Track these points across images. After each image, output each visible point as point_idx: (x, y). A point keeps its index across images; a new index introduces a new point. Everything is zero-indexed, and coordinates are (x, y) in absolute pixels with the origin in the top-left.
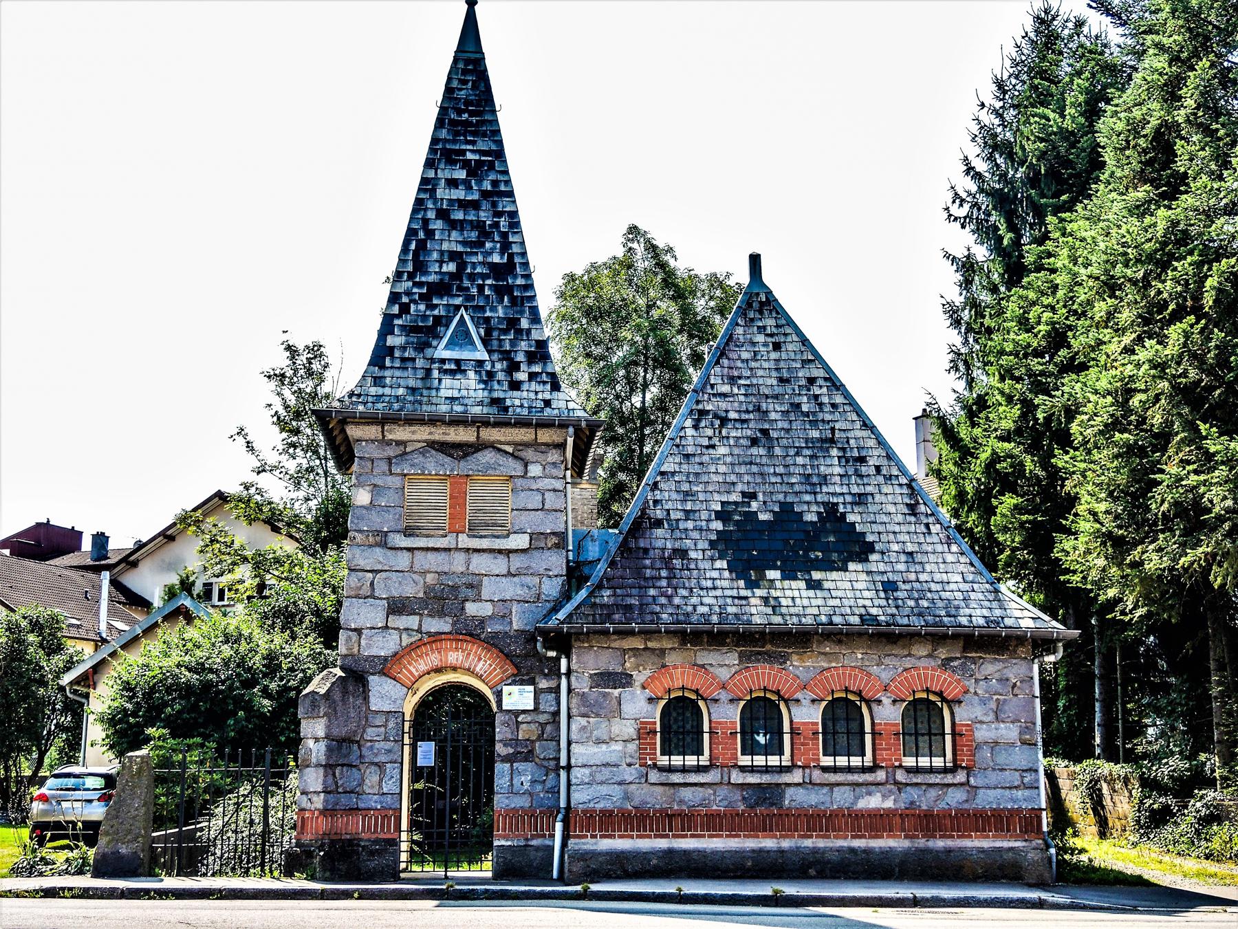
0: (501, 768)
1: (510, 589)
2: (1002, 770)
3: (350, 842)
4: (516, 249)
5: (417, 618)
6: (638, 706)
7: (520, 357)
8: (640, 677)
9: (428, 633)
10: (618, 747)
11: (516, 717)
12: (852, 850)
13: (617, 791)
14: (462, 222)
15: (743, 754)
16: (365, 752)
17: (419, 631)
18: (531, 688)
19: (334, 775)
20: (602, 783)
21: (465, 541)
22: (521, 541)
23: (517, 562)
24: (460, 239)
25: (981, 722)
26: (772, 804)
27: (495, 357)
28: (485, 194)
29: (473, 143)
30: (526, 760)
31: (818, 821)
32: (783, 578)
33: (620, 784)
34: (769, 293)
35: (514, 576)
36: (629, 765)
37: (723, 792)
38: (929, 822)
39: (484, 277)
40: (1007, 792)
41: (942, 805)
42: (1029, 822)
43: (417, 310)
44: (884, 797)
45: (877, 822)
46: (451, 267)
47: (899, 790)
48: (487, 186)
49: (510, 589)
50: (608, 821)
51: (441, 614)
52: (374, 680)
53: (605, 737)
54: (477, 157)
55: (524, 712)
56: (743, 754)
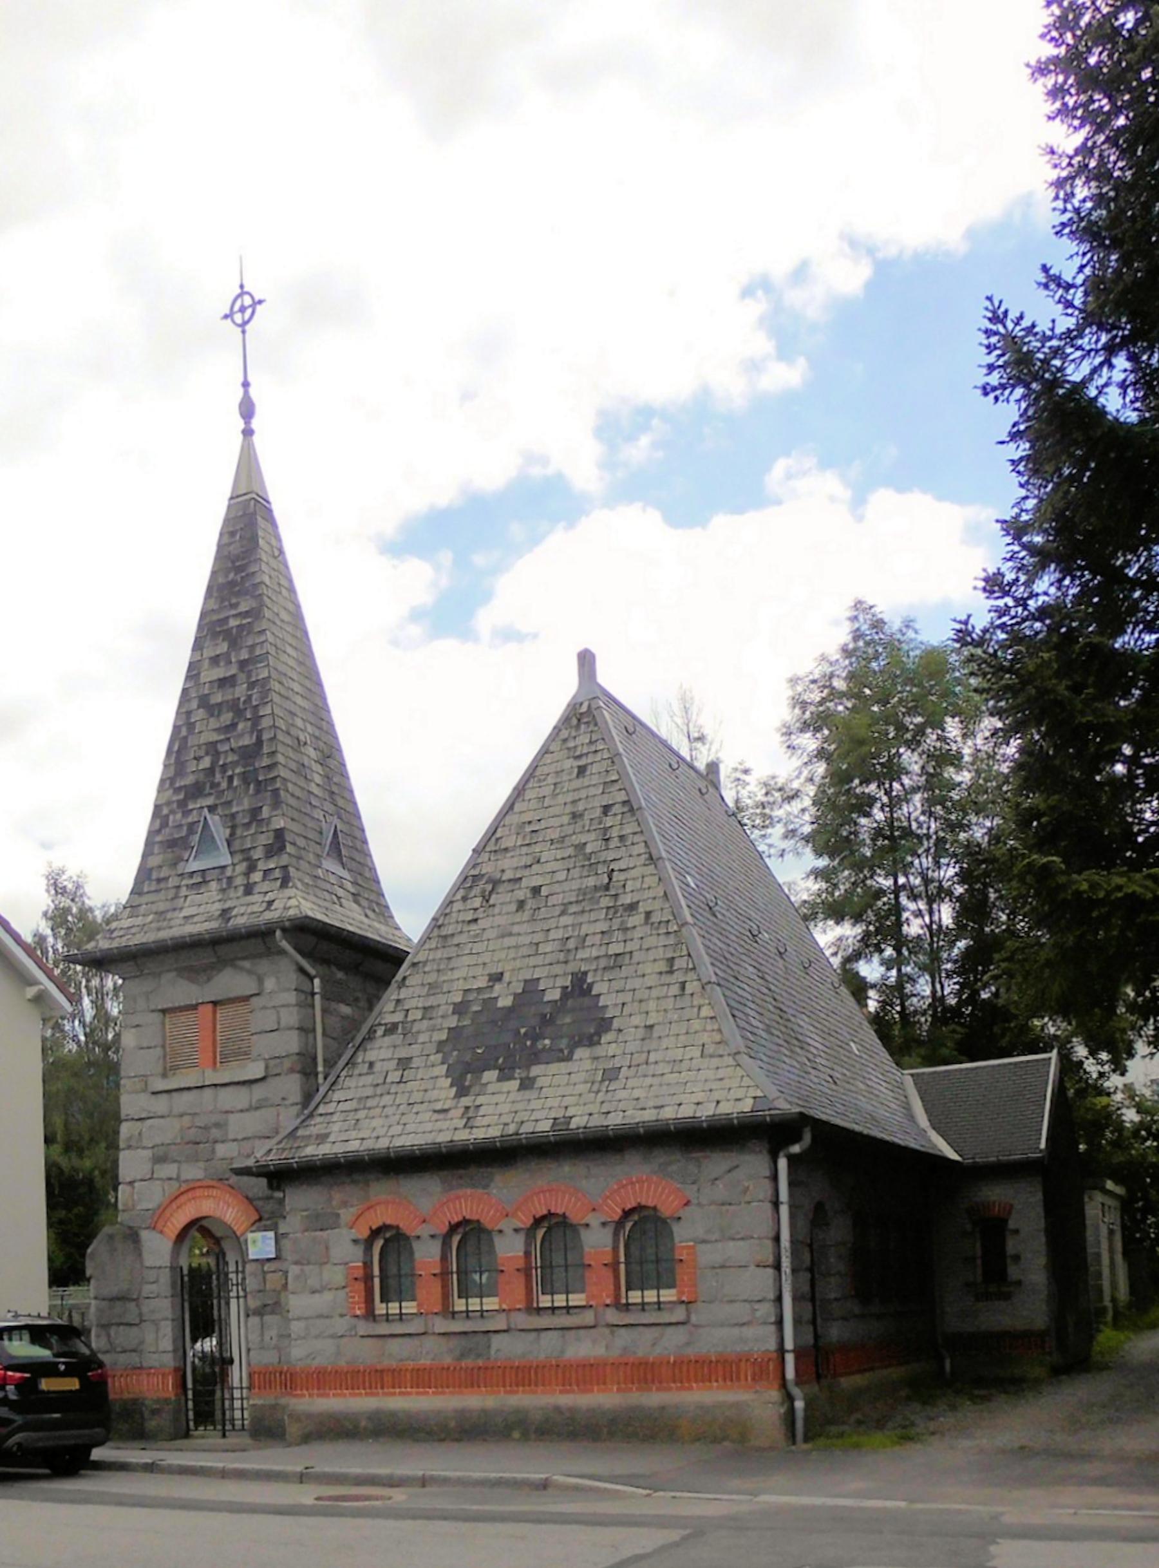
0: (170, 1348)
1: (252, 1123)
2: (732, 1301)
3: (135, 1401)
4: (265, 723)
5: (175, 1165)
6: (344, 1248)
7: (258, 854)
8: (346, 1215)
9: (186, 1181)
10: (328, 1296)
11: (263, 1266)
12: (558, 1409)
13: (789, 1107)
14: (220, 705)
15: (459, 1297)
16: (145, 1309)
17: (178, 1179)
18: (271, 1234)
19: (109, 1336)
20: (317, 1337)
21: (211, 1077)
22: (255, 1070)
23: (259, 1092)
24: (217, 726)
25: (704, 1241)
26: (479, 1356)
27: (238, 857)
28: (243, 664)
29: (234, 606)
30: (273, 1313)
31: (525, 1375)
32: (500, 1079)
33: (332, 1336)
34: (198, 646)
35: (257, 1108)
36: (342, 1316)
37: (430, 1343)
38: (645, 1373)
39: (235, 764)
40: (736, 1331)
41: (658, 1350)
42: (504, 1373)
43: (174, 821)
44: (594, 1342)
45: (588, 1374)
46: (206, 763)
47: (612, 1333)
48: (244, 655)
49: (252, 1123)
50: (323, 1379)
51: (194, 1159)
52: (145, 1235)
53: (318, 1287)
54: (237, 623)
55: (269, 1260)
56: (459, 1297)
